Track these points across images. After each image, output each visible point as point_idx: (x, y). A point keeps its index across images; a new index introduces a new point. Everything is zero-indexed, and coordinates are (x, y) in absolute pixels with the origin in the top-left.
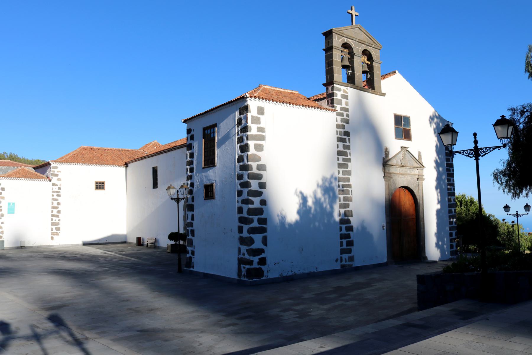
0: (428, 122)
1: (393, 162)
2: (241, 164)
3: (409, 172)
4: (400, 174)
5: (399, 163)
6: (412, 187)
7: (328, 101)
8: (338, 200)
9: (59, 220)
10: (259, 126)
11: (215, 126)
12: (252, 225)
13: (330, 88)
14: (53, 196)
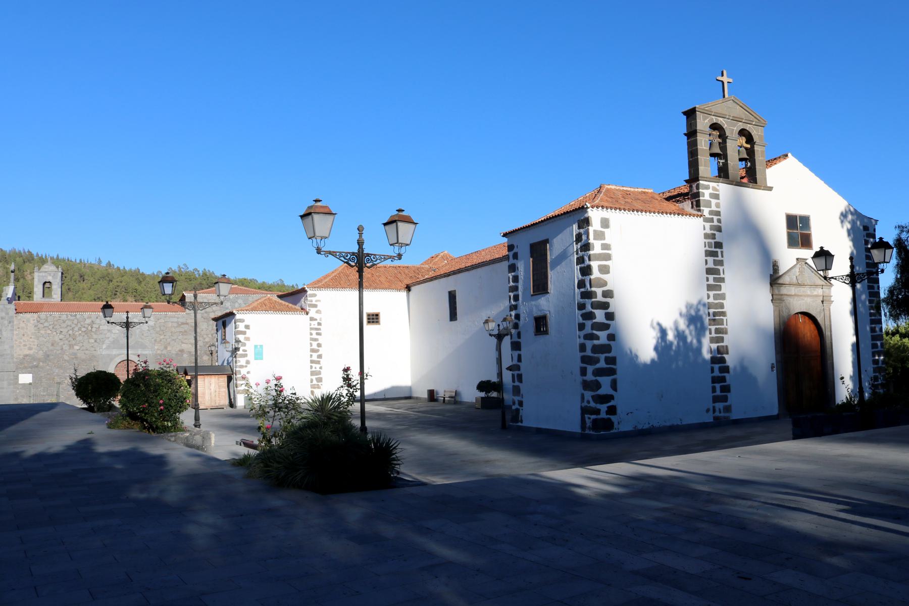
0: (839, 221)
1: (786, 280)
2: (582, 290)
3: (809, 293)
4: (795, 295)
5: (795, 281)
6: (813, 313)
8: (707, 333)
9: (321, 368)
11: (546, 242)
13: (694, 186)
14: (311, 334)
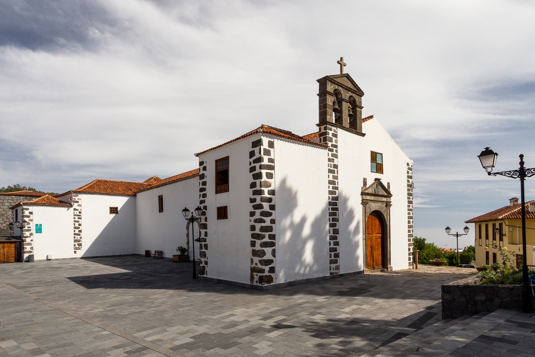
7: (320, 139)
9: (81, 238)
10: (270, 157)
12: (264, 240)
14: (75, 218)
